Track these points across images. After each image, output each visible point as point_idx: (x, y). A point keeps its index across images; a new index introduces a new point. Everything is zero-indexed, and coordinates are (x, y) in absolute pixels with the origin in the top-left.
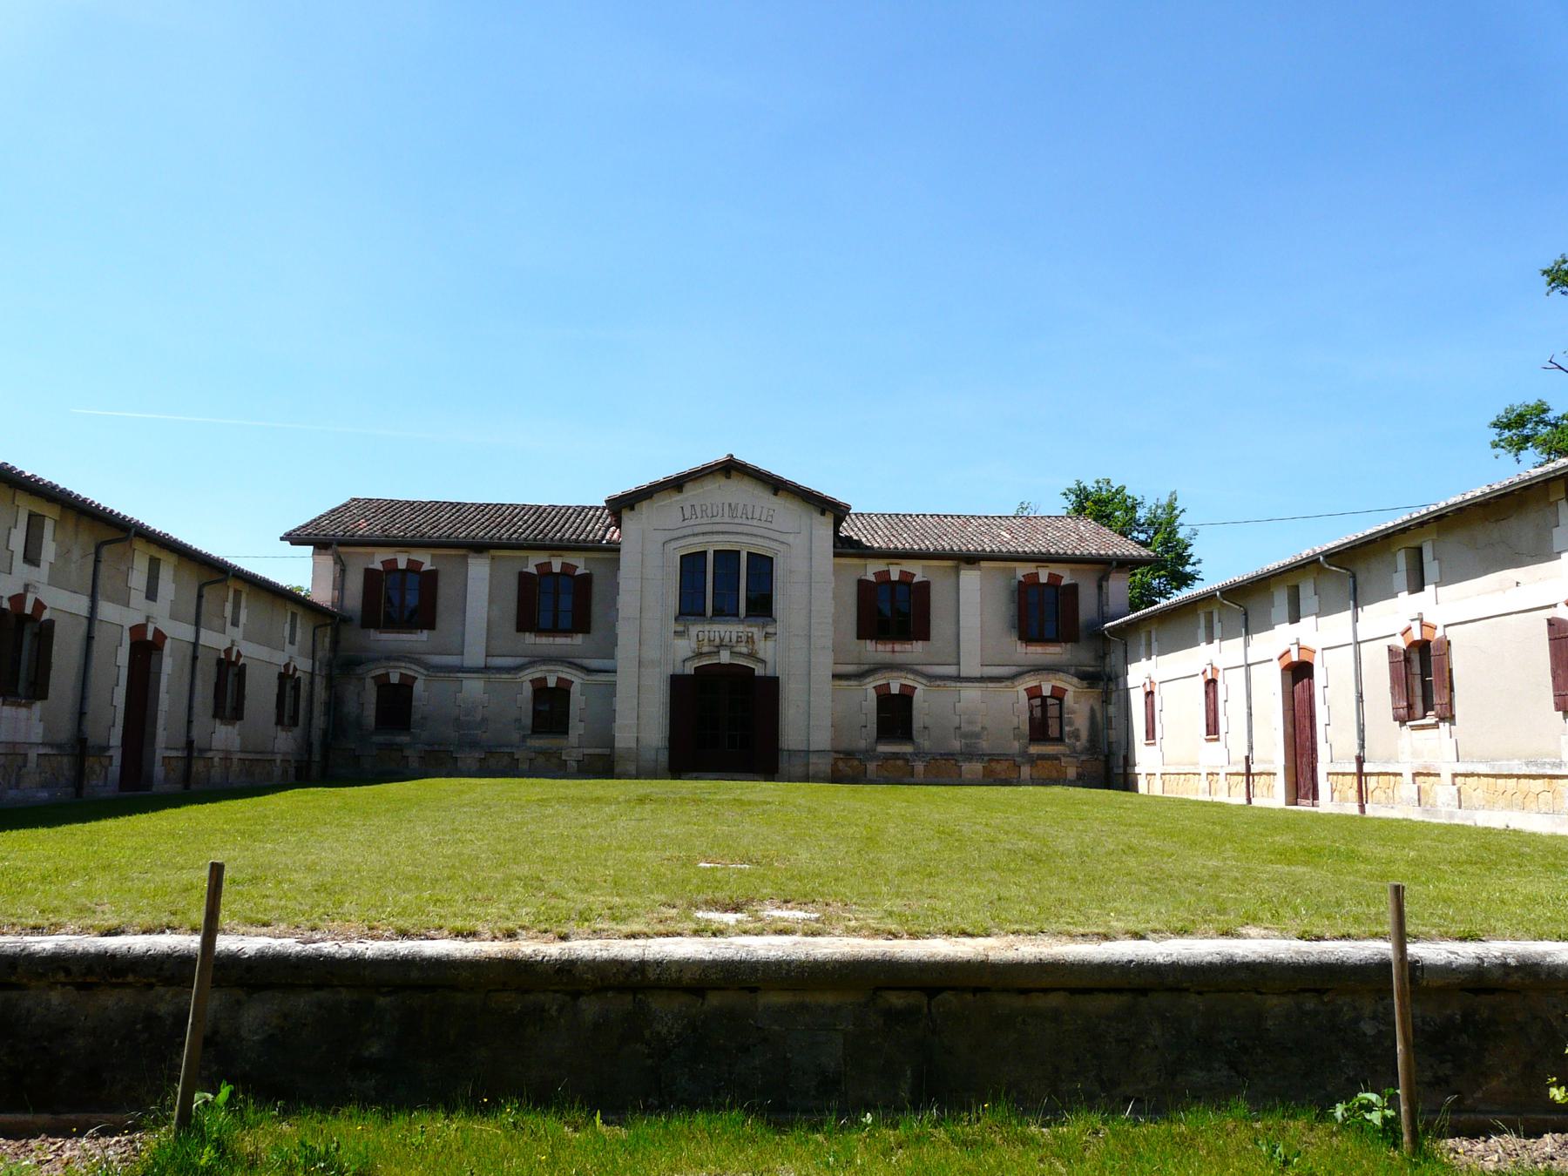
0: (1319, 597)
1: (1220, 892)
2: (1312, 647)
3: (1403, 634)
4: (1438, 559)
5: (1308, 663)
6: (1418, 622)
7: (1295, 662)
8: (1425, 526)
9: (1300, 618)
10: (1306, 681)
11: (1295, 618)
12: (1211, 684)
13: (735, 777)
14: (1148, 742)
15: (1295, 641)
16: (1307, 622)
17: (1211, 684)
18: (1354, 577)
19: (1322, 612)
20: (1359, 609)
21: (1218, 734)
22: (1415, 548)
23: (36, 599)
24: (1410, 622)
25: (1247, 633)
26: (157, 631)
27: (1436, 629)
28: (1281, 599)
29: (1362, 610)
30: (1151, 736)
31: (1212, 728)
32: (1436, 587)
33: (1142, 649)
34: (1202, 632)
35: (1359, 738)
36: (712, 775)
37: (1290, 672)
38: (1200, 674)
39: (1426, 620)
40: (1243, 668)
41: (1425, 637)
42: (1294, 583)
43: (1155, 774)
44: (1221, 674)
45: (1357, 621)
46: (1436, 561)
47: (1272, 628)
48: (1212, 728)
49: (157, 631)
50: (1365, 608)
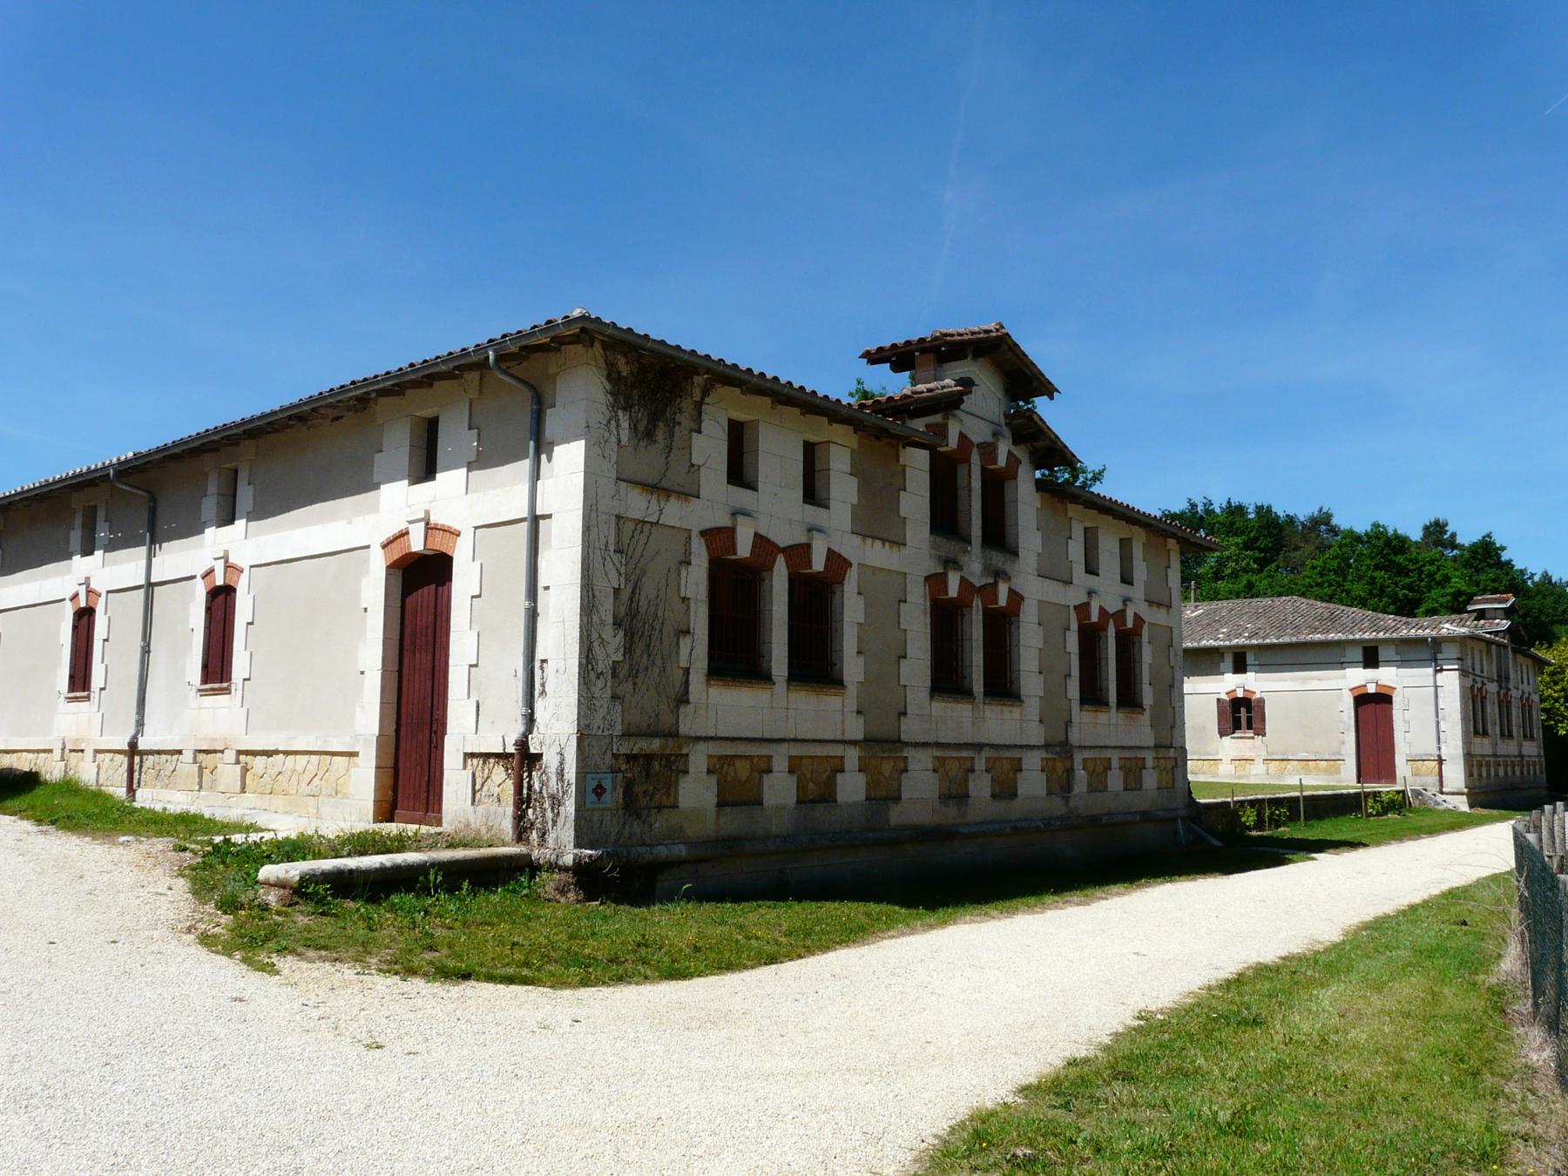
0: (254, 487)
1: (1065, 1137)
2: (455, 525)
3: (71, 600)
4: (110, 522)
5: (233, 587)
6: (222, 561)
7: (415, 553)
8: (437, 384)
9: (234, 520)
10: (433, 586)
11: (426, 470)
12: (84, 618)
13: (443, 665)
14: (72, 695)
15: (422, 515)
16: (450, 480)
17: (84, 618)
18: (153, 500)
19: (481, 461)
20: (544, 457)
21: (89, 689)
22: (231, 470)
23: (830, 551)
24: (407, 525)
25: (153, 541)
26: (832, 555)
27: (242, 572)
28: (398, 443)
29: (160, 547)
30: (79, 682)
31: (80, 679)
32: (468, 471)
33: (209, 505)
34: (76, 537)
35: (138, 713)
36: (1008, 507)
37: (401, 571)
38: (199, 577)
39: (433, 520)
40: (142, 590)
41: (228, 582)
42: (428, 413)
43: (180, 752)
44: (102, 601)
45: (538, 479)
46: (108, 523)
47: (376, 487)
48: (80, 679)
49: (832, 555)
50: (164, 545)
